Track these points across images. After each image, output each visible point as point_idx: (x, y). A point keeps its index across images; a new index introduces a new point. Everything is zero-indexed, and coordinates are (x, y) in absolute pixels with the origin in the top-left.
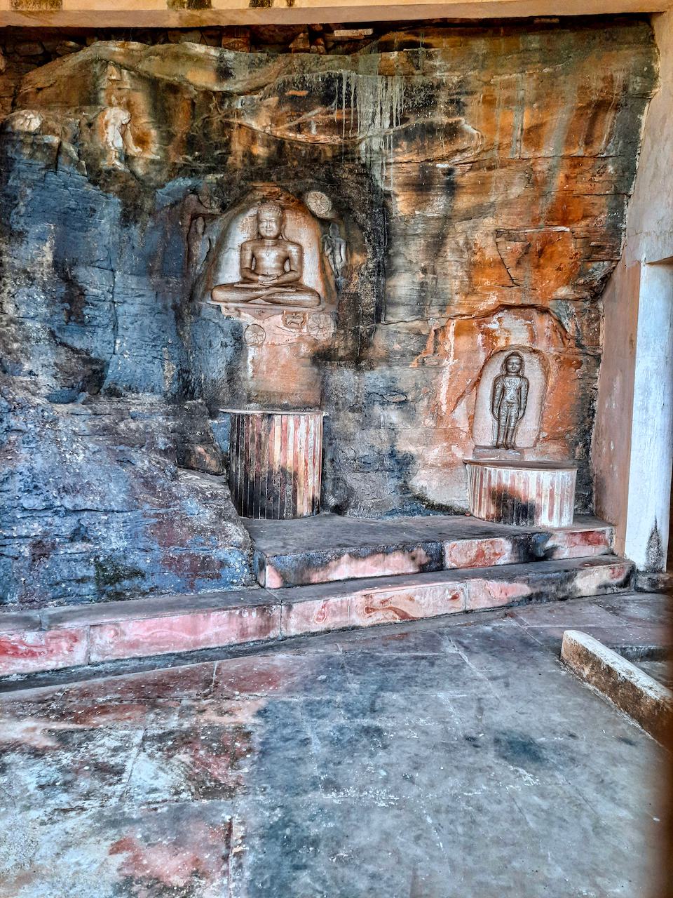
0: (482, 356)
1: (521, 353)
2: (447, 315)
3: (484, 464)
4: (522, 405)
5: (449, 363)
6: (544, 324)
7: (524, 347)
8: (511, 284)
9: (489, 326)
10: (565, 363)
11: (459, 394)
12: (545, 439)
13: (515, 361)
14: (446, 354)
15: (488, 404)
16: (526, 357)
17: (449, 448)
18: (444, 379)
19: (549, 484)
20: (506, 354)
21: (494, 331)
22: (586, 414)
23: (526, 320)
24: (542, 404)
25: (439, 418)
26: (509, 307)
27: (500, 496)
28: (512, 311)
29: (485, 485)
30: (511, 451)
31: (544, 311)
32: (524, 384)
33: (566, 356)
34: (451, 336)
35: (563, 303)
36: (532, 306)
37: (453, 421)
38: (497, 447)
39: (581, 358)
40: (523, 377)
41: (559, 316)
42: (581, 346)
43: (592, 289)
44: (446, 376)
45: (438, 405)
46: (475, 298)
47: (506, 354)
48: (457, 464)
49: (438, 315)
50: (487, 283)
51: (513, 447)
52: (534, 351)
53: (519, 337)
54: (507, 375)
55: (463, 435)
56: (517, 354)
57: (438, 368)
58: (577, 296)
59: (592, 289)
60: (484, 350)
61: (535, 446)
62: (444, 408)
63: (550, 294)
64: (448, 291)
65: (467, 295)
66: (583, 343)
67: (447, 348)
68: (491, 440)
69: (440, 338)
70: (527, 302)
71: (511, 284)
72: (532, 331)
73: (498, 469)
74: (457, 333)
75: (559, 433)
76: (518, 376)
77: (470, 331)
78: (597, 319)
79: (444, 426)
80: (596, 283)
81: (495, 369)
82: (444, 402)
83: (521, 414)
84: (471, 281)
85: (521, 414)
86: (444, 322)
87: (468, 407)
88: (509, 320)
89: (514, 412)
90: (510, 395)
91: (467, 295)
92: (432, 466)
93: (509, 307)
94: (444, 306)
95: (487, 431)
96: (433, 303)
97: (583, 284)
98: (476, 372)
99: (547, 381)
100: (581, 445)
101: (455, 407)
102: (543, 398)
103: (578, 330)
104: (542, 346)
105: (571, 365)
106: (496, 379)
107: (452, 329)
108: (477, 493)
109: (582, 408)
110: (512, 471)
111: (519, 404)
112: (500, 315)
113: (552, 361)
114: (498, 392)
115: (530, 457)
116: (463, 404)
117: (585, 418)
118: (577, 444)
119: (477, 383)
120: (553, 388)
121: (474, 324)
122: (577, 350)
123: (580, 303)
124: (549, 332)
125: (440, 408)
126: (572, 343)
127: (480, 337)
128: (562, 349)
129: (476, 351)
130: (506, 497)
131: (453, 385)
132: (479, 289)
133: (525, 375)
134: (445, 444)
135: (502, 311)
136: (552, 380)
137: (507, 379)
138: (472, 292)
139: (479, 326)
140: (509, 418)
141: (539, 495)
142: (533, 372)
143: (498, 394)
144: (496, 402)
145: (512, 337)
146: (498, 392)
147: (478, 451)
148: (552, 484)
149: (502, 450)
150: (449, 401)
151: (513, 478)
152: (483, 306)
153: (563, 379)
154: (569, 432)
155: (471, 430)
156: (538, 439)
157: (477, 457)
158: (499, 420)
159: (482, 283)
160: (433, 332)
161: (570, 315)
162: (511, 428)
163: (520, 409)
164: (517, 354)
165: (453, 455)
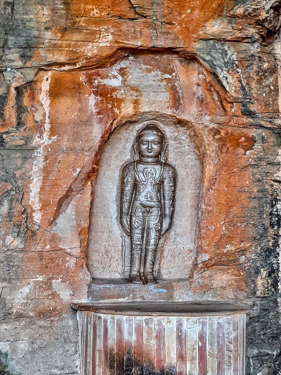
0: (97, 132)
1: (161, 126)
2: (34, 62)
3: (96, 309)
4: (166, 215)
5: (43, 140)
6: (191, 78)
7: (163, 116)
8: (132, 15)
9: (105, 82)
10: (228, 141)
11: (61, 193)
12: (207, 265)
13: (150, 138)
14: (39, 127)
15: (113, 209)
16: (169, 131)
17: (47, 284)
18: (35, 169)
19: (196, 337)
20: (139, 126)
21: (114, 89)
22: (267, 223)
23: (165, 72)
24: (197, 208)
25: (29, 234)
26: (136, 52)
27: (121, 363)
28: (141, 58)
29: (100, 344)
30: (151, 287)
31: (191, 58)
32: (168, 175)
33: (230, 130)
34: (44, 99)
35: (218, 46)
36: (170, 51)
37: (54, 238)
38: (130, 280)
39: (253, 132)
40: (166, 164)
41: (213, 66)
42: (250, 114)
43: (260, 23)
44: (38, 164)
45: (27, 212)
46: (76, 37)
47: (139, 126)
48: (60, 313)
49: (19, 64)
50: (95, 12)
51: (155, 280)
52: (180, 123)
53: (156, 102)
54: (140, 162)
55: (71, 262)
56: (154, 128)
57: (26, 151)
58: (239, 35)
59: (260, 23)
60: (101, 121)
61: (191, 276)
62: (37, 217)
63: (195, 31)
64: (32, 24)
65: (64, 30)
66: (253, 108)
67: (38, 117)
68: (120, 269)
69: (26, 101)
70: (161, 43)
71: (132, 15)
72: (173, 90)
73: (117, 317)
74: (55, 93)
75: (227, 254)
76: (158, 162)
77: (77, 89)
78: (273, 70)
79: (39, 248)
80: (264, 15)
81: (122, 151)
82: (37, 206)
83: (165, 225)
84: (68, 9)
85: (165, 225)
86: (30, 75)
87: (78, 213)
88: (137, 71)
89: (153, 221)
90: (147, 193)
91: (64, 30)
92: (20, 316)
93: (136, 52)
94: (28, 49)
95: (112, 257)
96: (10, 43)
97: (244, 16)
98: (88, 158)
99: (203, 172)
100: (264, 273)
101: (56, 215)
102: (199, 198)
103: (243, 88)
104: (190, 113)
105: (238, 145)
106: (125, 168)
107: (45, 86)
108: (90, 360)
109: (261, 213)
110: (139, 319)
111: (161, 208)
112: (123, 64)
113: (207, 138)
114: (128, 188)
115: (183, 296)
116: (70, 210)
117: (266, 230)
118: (257, 272)
119: (93, 174)
120: (213, 182)
121: (82, 78)
122: (246, 120)
123: (244, 46)
124: (200, 92)
125: (29, 217)
126: (235, 109)
127: (92, 100)
128: (222, 119)
129: (87, 123)
130: (131, 363)
131: (52, 177)
132: (82, 22)
133: (171, 161)
134: (40, 279)
135: (126, 58)
136: (210, 169)
137: (141, 167)
138: (73, 28)
139: (90, 81)
140: (145, 230)
141: (181, 357)
142: (181, 153)
143: (128, 191)
144: (126, 205)
145: (143, 99)
146: (128, 188)
147: (96, 287)
148: (202, 338)
149: (135, 286)
150: (45, 205)
151: (139, 330)
152: (90, 50)
153: (226, 167)
154: (243, 252)
155: (86, 254)
156: (195, 265)
157: (95, 297)
158: (130, 235)
159: (86, 13)
160: (13, 92)
161: (230, 65)
162: (151, 247)
163: (162, 216)
164: (154, 128)
165: (54, 295)
